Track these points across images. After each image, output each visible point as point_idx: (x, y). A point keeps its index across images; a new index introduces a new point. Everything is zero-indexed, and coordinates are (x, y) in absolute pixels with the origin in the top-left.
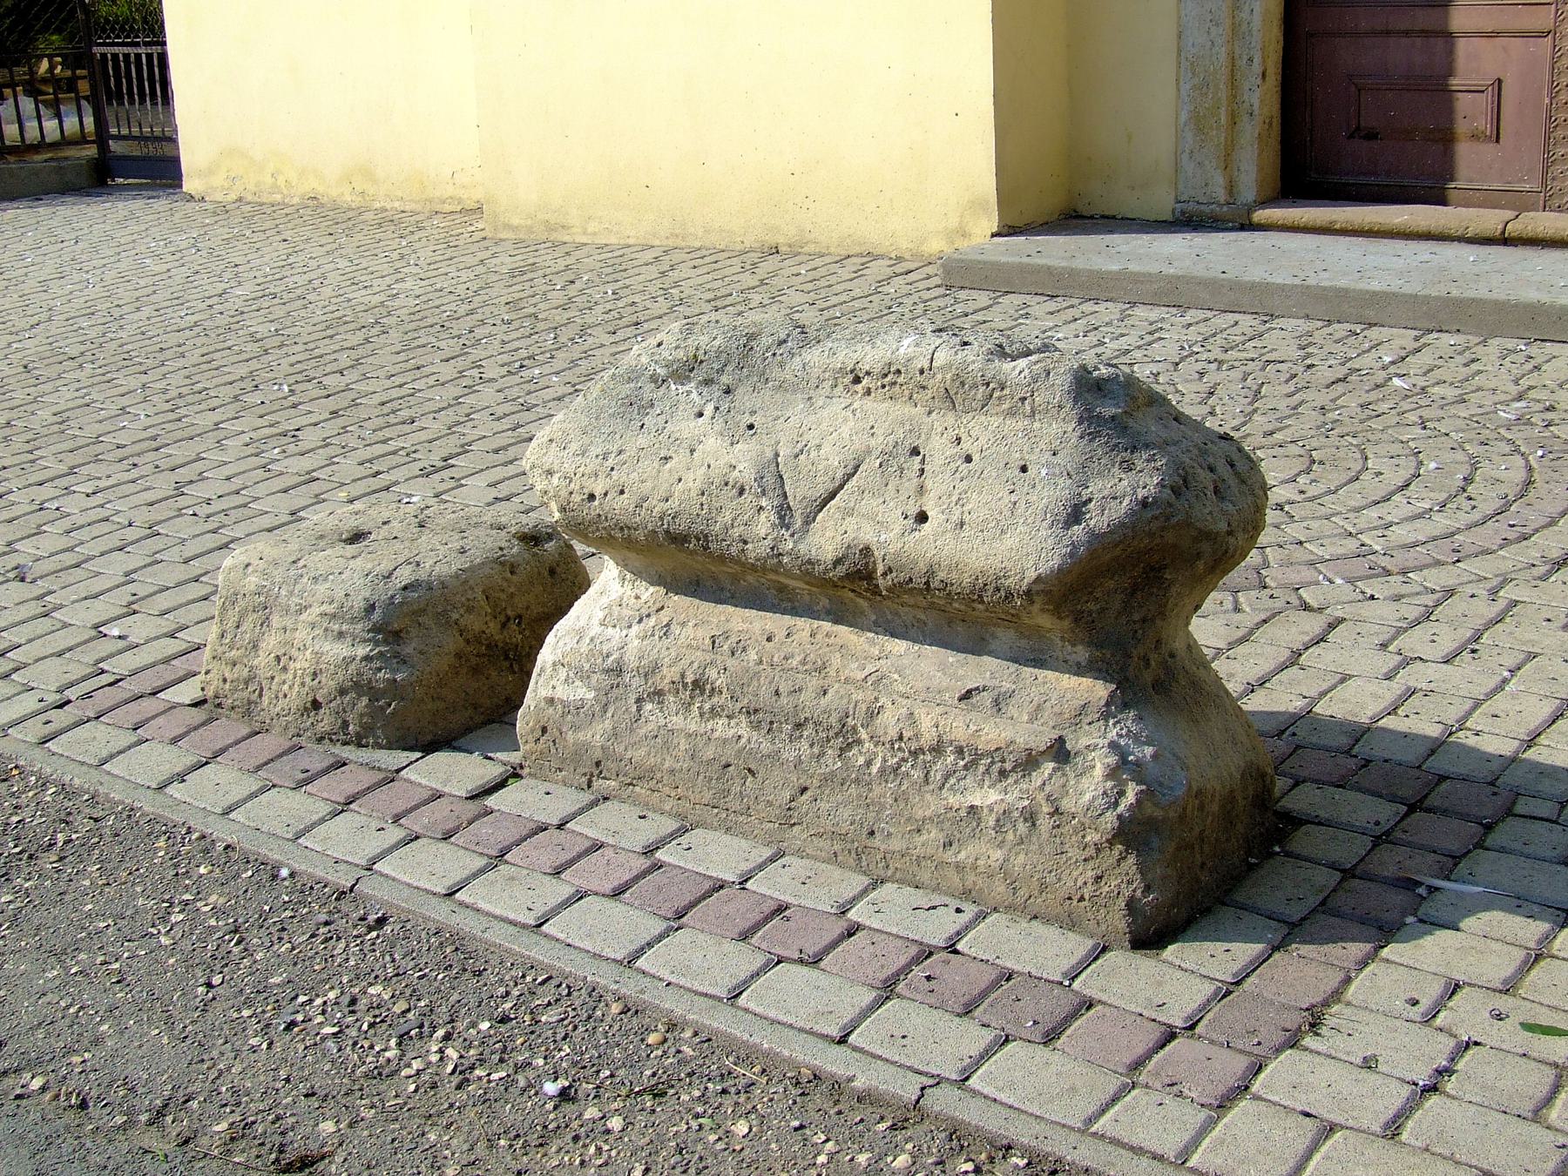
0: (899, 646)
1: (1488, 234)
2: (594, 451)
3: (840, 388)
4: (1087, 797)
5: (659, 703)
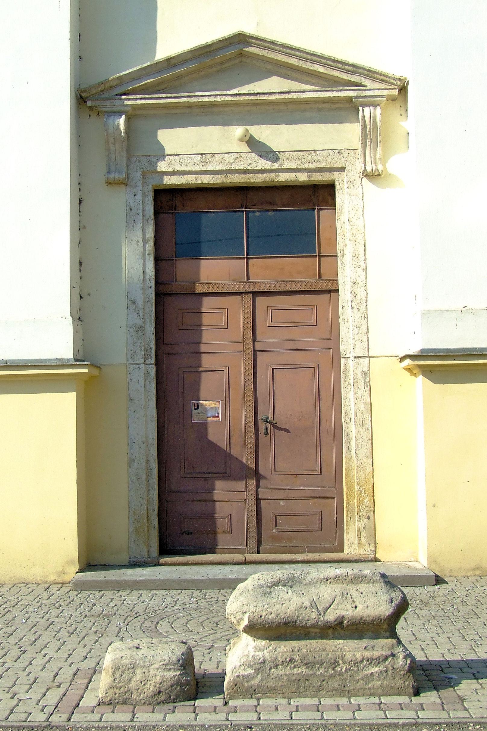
0: (341, 641)
1: (240, 561)
2: (259, 605)
3: (323, 582)
4: (400, 663)
5: (276, 668)
